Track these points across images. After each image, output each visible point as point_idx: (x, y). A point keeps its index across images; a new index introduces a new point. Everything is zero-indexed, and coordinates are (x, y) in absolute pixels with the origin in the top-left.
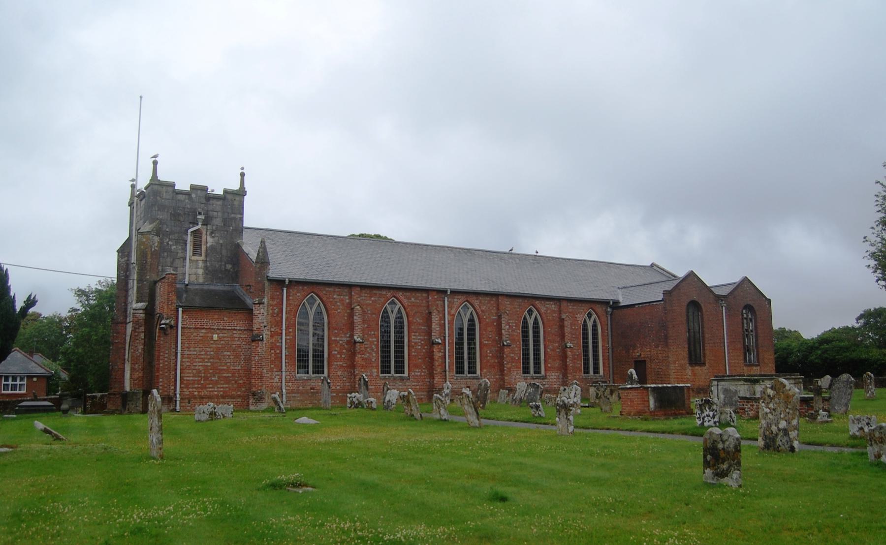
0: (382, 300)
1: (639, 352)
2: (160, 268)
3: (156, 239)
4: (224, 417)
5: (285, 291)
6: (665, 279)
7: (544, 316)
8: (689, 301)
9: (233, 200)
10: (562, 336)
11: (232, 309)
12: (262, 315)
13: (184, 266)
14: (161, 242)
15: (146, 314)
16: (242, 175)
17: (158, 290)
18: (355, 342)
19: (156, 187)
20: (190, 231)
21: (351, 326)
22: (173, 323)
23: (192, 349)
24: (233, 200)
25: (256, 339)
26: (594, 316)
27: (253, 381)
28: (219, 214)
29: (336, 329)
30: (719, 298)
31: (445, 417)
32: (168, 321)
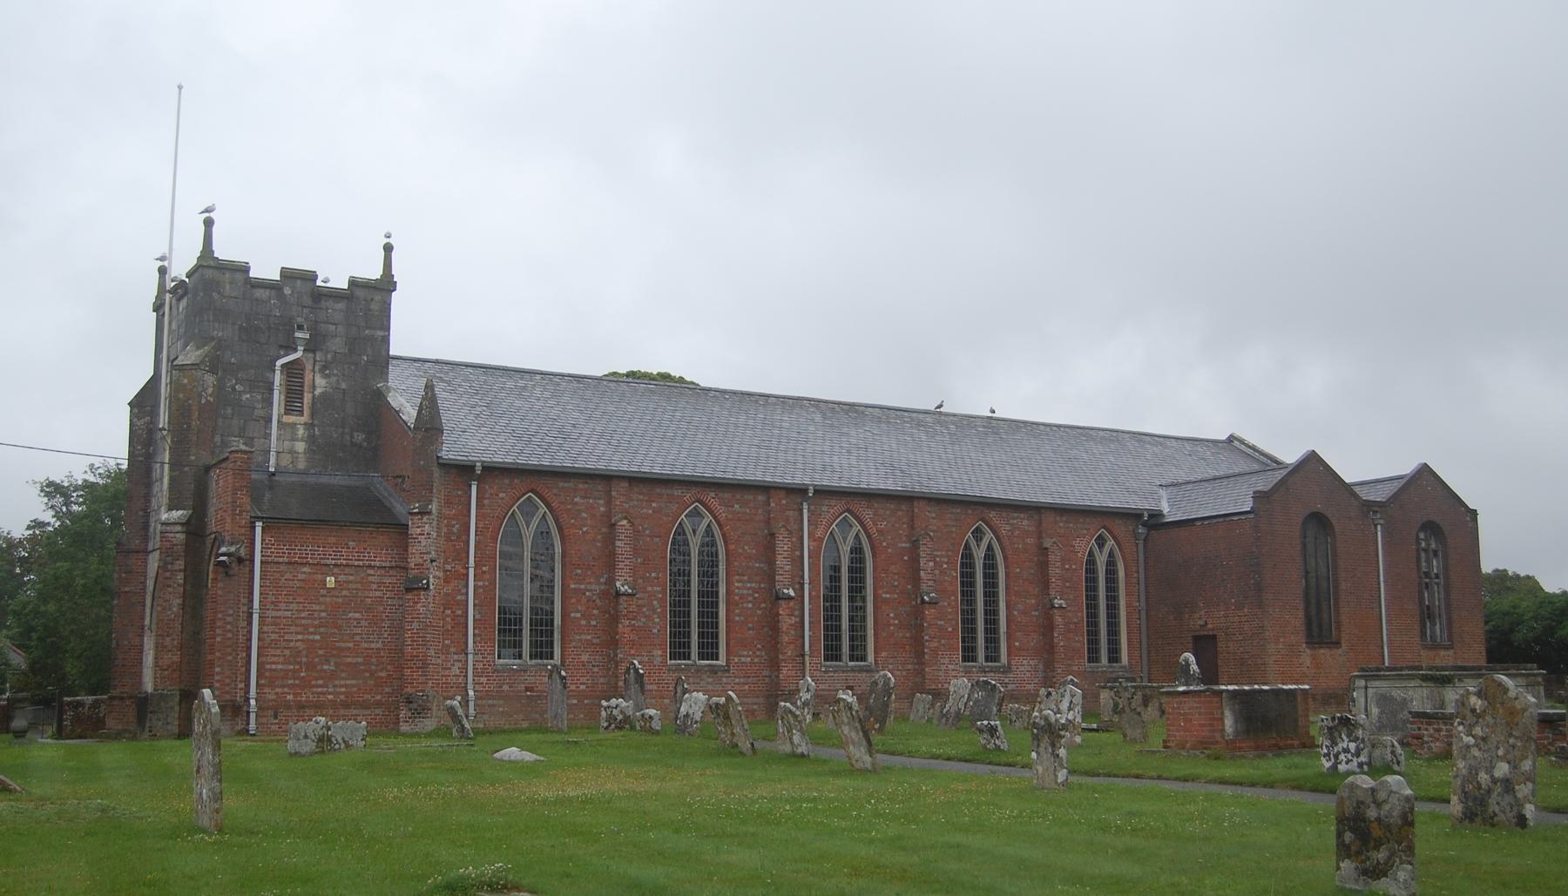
2: (218, 439)
3: (210, 380)
4: (348, 746)
5: (474, 488)
6: (1242, 466)
7: (1006, 542)
9: (370, 300)
10: (1045, 584)
11: (361, 524)
12: (426, 536)
13: (268, 436)
14: (220, 387)
16: (388, 249)
18: (618, 594)
19: (209, 273)
20: (279, 363)
22: (243, 552)
23: (282, 606)
24: (370, 300)
25: (414, 586)
26: (1111, 543)
30: (1369, 506)
32: (233, 549)
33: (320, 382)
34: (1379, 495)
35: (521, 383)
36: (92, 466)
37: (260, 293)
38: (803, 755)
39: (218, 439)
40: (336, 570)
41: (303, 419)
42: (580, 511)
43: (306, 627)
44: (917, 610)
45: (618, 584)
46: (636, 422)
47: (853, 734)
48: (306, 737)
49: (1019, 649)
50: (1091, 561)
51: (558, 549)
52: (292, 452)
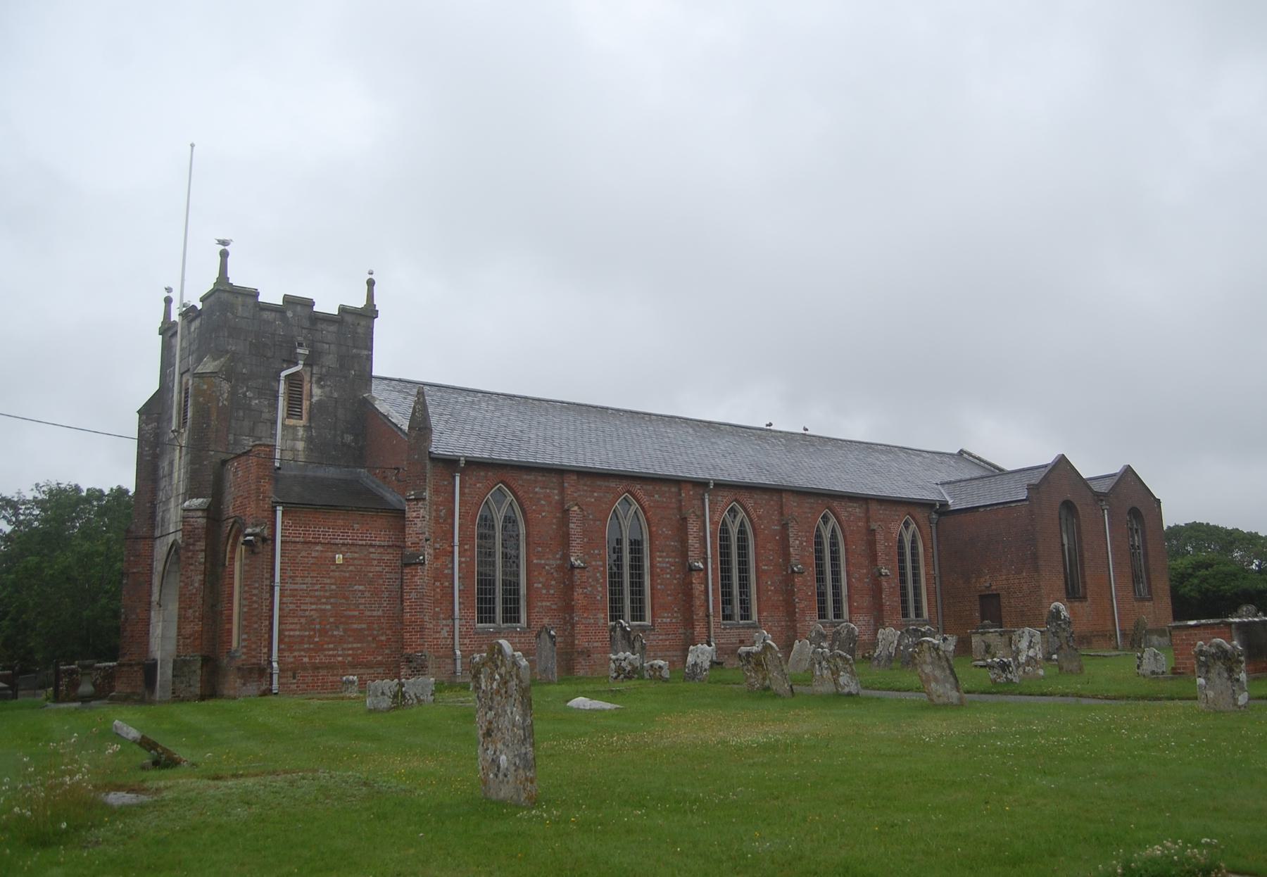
0: (611, 496)
1: (986, 582)
2: (231, 437)
3: (226, 386)
4: (419, 701)
5: (458, 479)
6: (977, 473)
7: (845, 524)
8: (1061, 500)
9: (356, 326)
10: (873, 558)
11: (366, 509)
12: (420, 519)
13: (274, 436)
14: (233, 393)
15: (208, 518)
16: (371, 283)
17: (230, 477)
18: (573, 567)
19: (225, 296)
20: (283, 374)
21: (565, 540)
22: (266, 532)
23: (299, 580)
24: (356, 326)
25: (410, 562)
26: (913, 526)
27: (407, 636)
28: (333, 347)
29: (539, 545)
30: (1099, 497)
31: (853, 688)
32: (258, 530)
33: (317, 391)
34: (1102, 488)
35: (469, 399)
36: (37, 485)
37: (266, 315)
38: (850, 694)
39: (231, 437)
40: (344, 549)
41: (302, 423)
42: (539, 499)
43: (319, 598)
44: (789, 578)
45: (572, 559)
46: (565, 430)
47: (937, 673)
48: (383, 693)
49: (857, 608)
50: (901, 541)
51: (522, 530)
52: (293, 449)
